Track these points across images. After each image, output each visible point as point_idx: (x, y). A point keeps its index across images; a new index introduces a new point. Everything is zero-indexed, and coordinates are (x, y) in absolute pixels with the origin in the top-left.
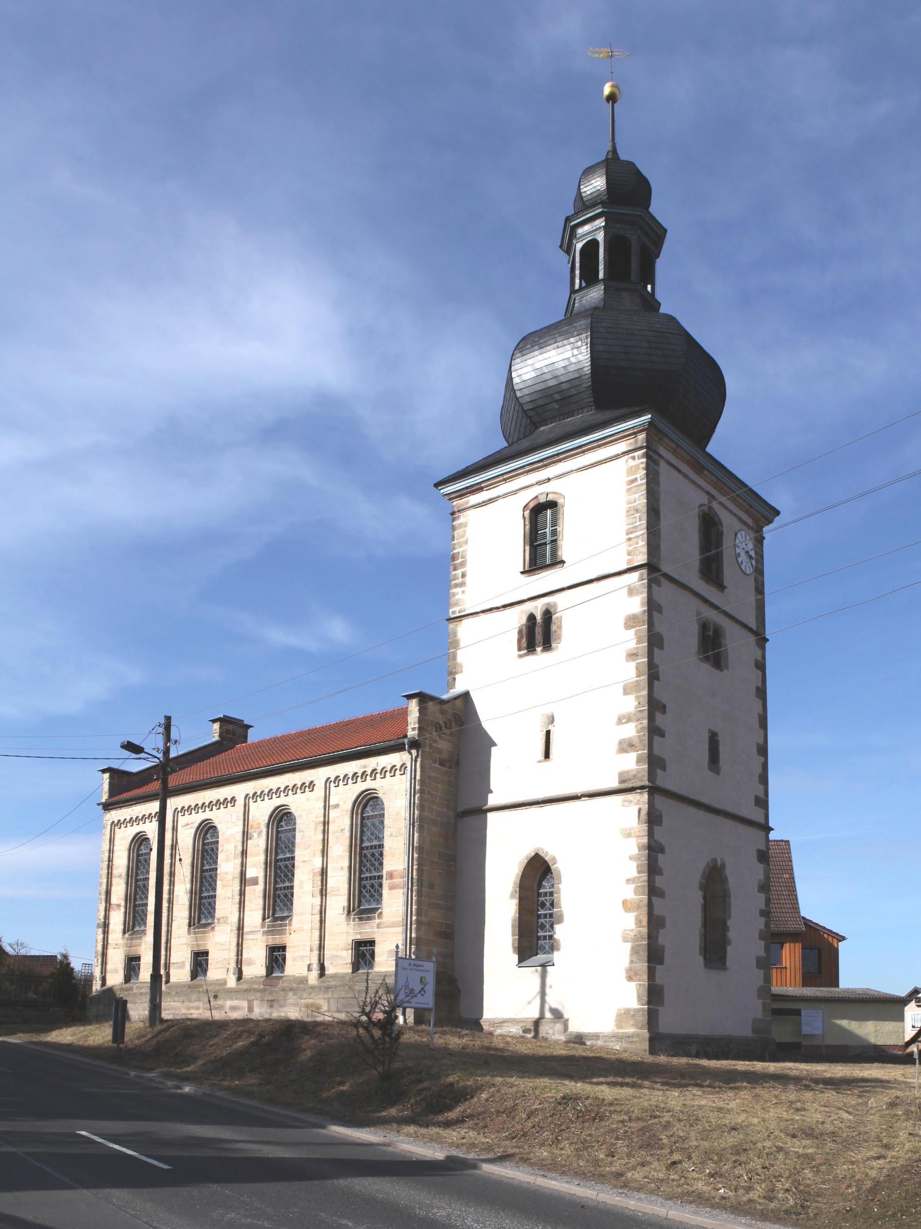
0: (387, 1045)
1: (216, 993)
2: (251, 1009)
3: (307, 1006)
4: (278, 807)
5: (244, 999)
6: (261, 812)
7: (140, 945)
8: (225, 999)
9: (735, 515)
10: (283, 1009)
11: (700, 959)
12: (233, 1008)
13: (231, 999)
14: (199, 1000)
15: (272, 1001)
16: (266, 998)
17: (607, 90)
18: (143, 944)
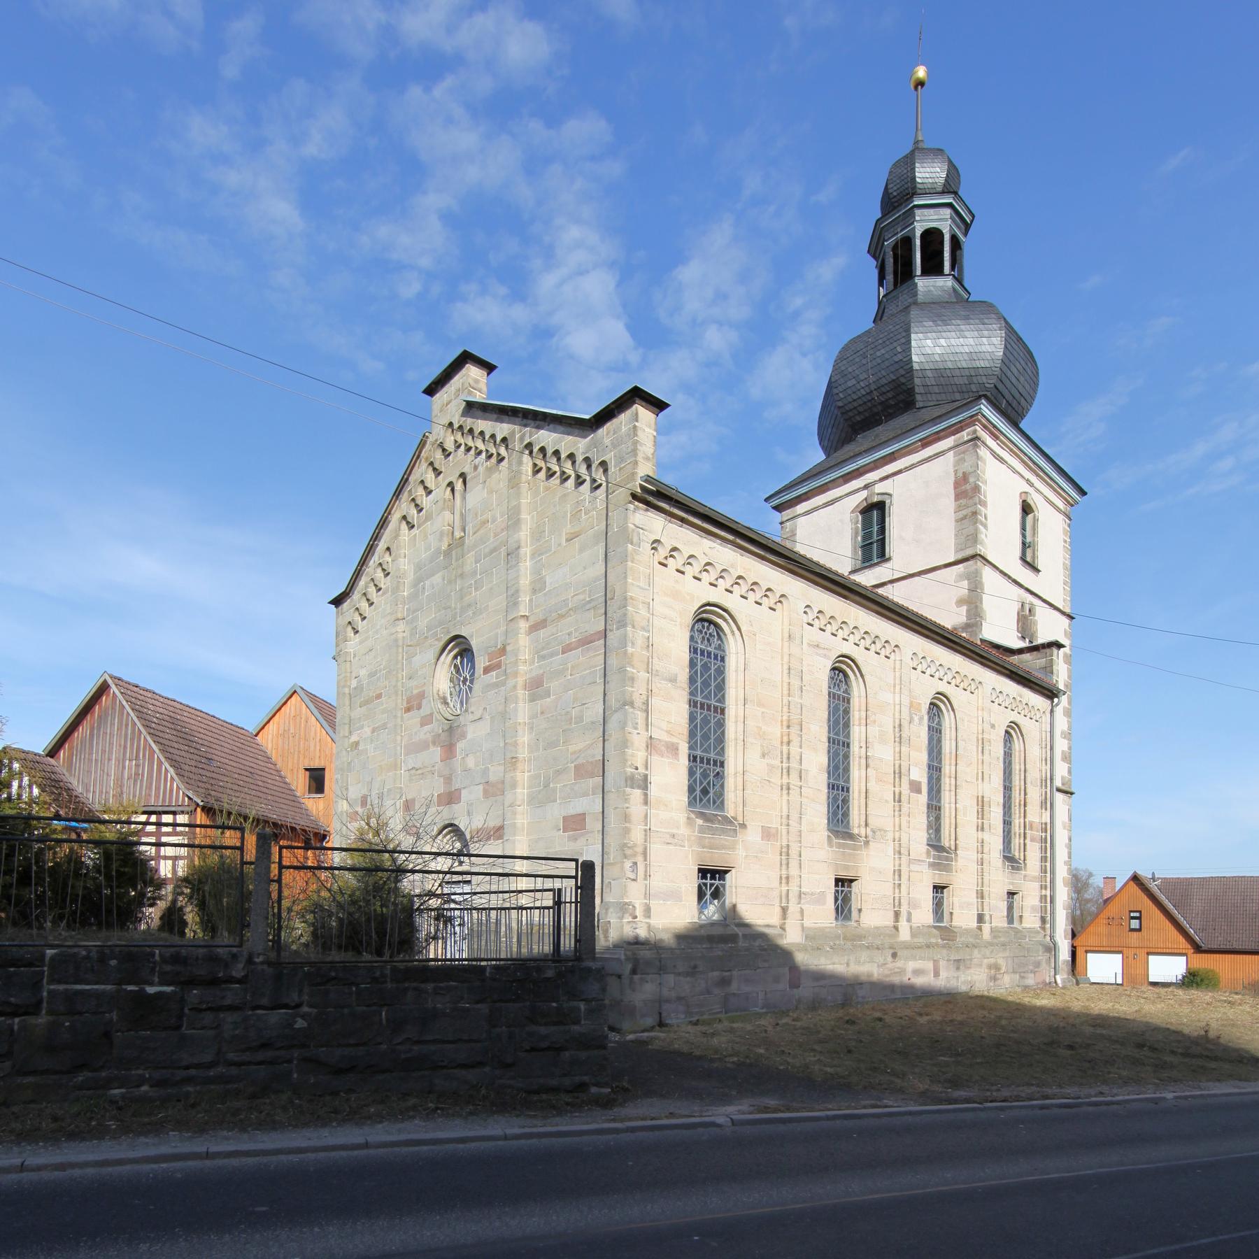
0: (181, 819)
1: (856, 941)
2: (937, 974)
3: (990, 967)
4: (853, 661)
5: (929, 959)
6: (925, 690)
7: (733, 848)
8: (907, 959)
9: (848, 495)
10: (968, 972)
11: (685, 798)
12: (917, 972)
13: (914, 958)
14: (872, 961)
15: (959, 961)
16: (952, 958)
17: (921, 72)
18: (740, 846)
